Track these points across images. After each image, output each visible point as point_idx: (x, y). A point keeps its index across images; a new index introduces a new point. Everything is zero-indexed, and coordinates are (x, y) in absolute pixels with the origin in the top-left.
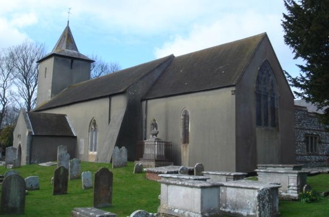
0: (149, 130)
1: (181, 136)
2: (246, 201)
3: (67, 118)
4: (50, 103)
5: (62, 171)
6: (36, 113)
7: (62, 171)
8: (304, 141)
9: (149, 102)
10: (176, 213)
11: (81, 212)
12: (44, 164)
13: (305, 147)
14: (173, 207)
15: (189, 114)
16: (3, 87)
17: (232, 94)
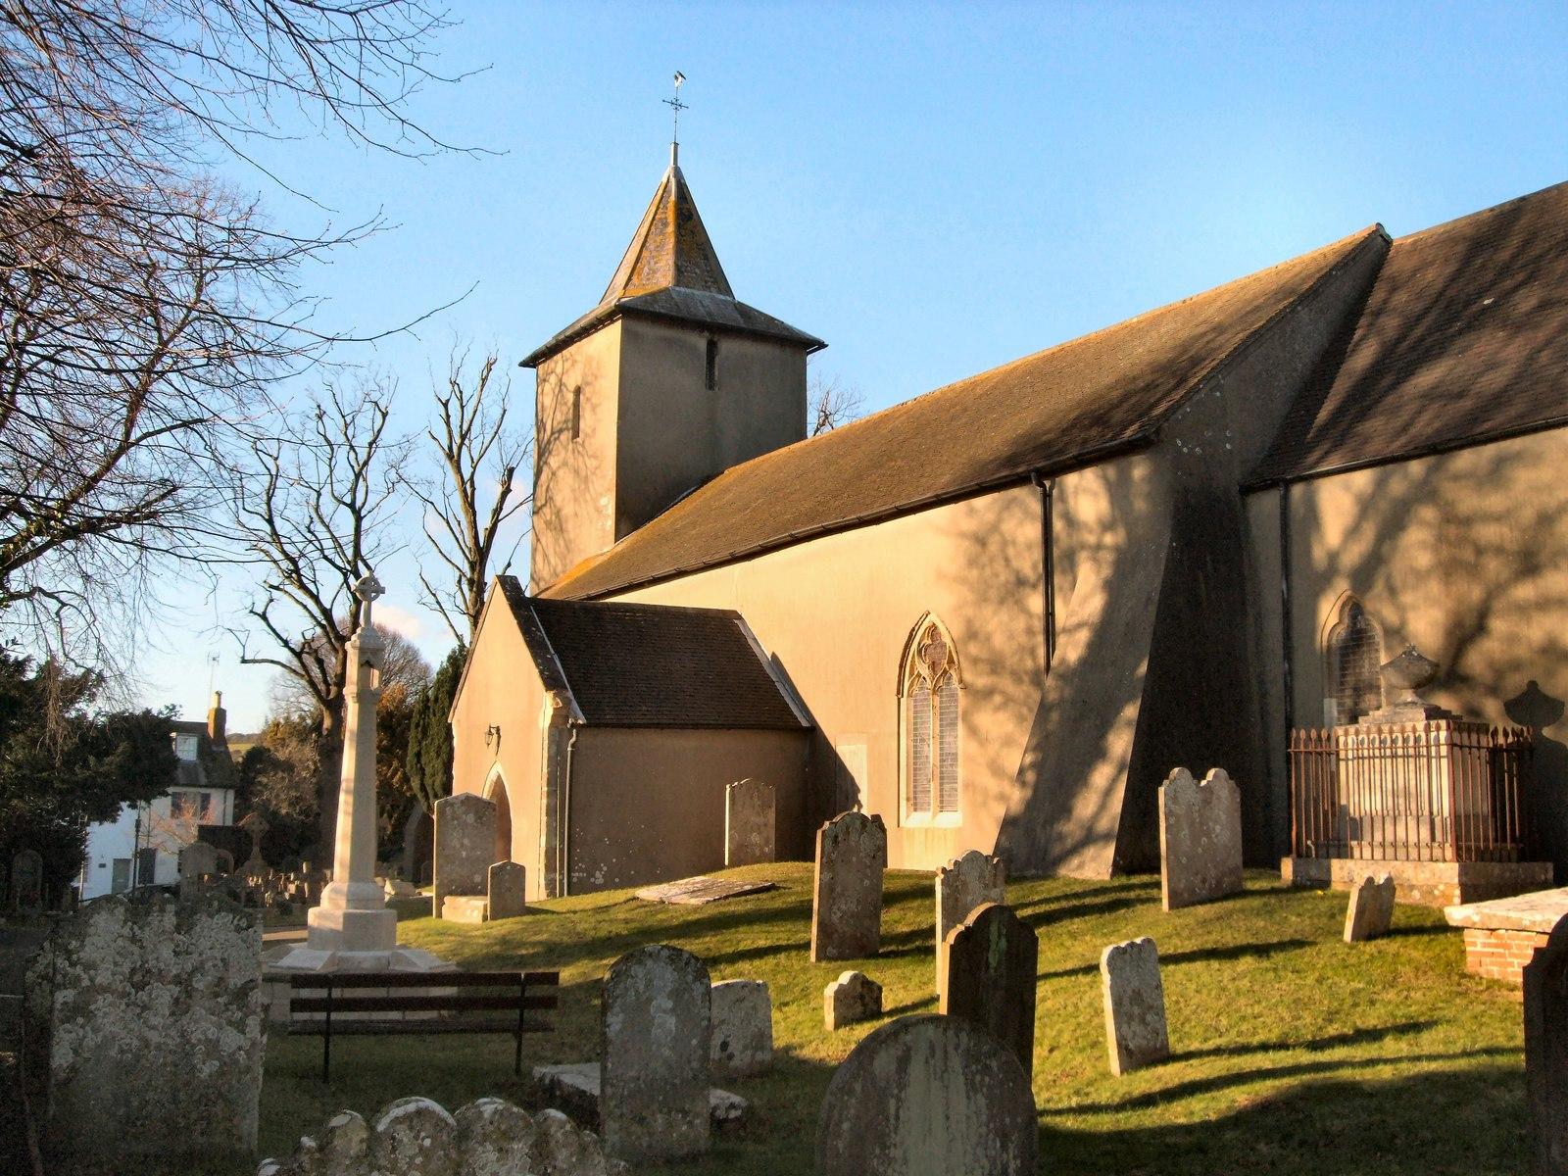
16: (352, 506)
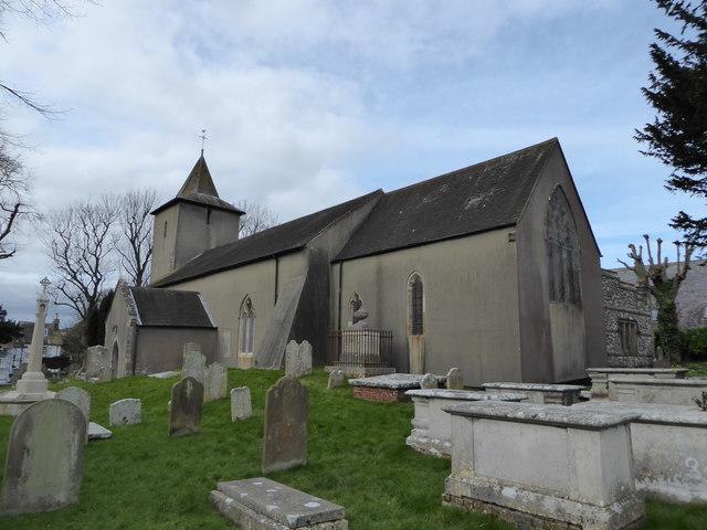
0: (347, 312)
1: (409, 322)
2: (683, 459)
5: (189, 388)
7: (189, 388)
8: (618, 331)
9: (345, 264)
10: (508, 499)
11: (238, 499)
12: (159, 375)
15: (423, 281)
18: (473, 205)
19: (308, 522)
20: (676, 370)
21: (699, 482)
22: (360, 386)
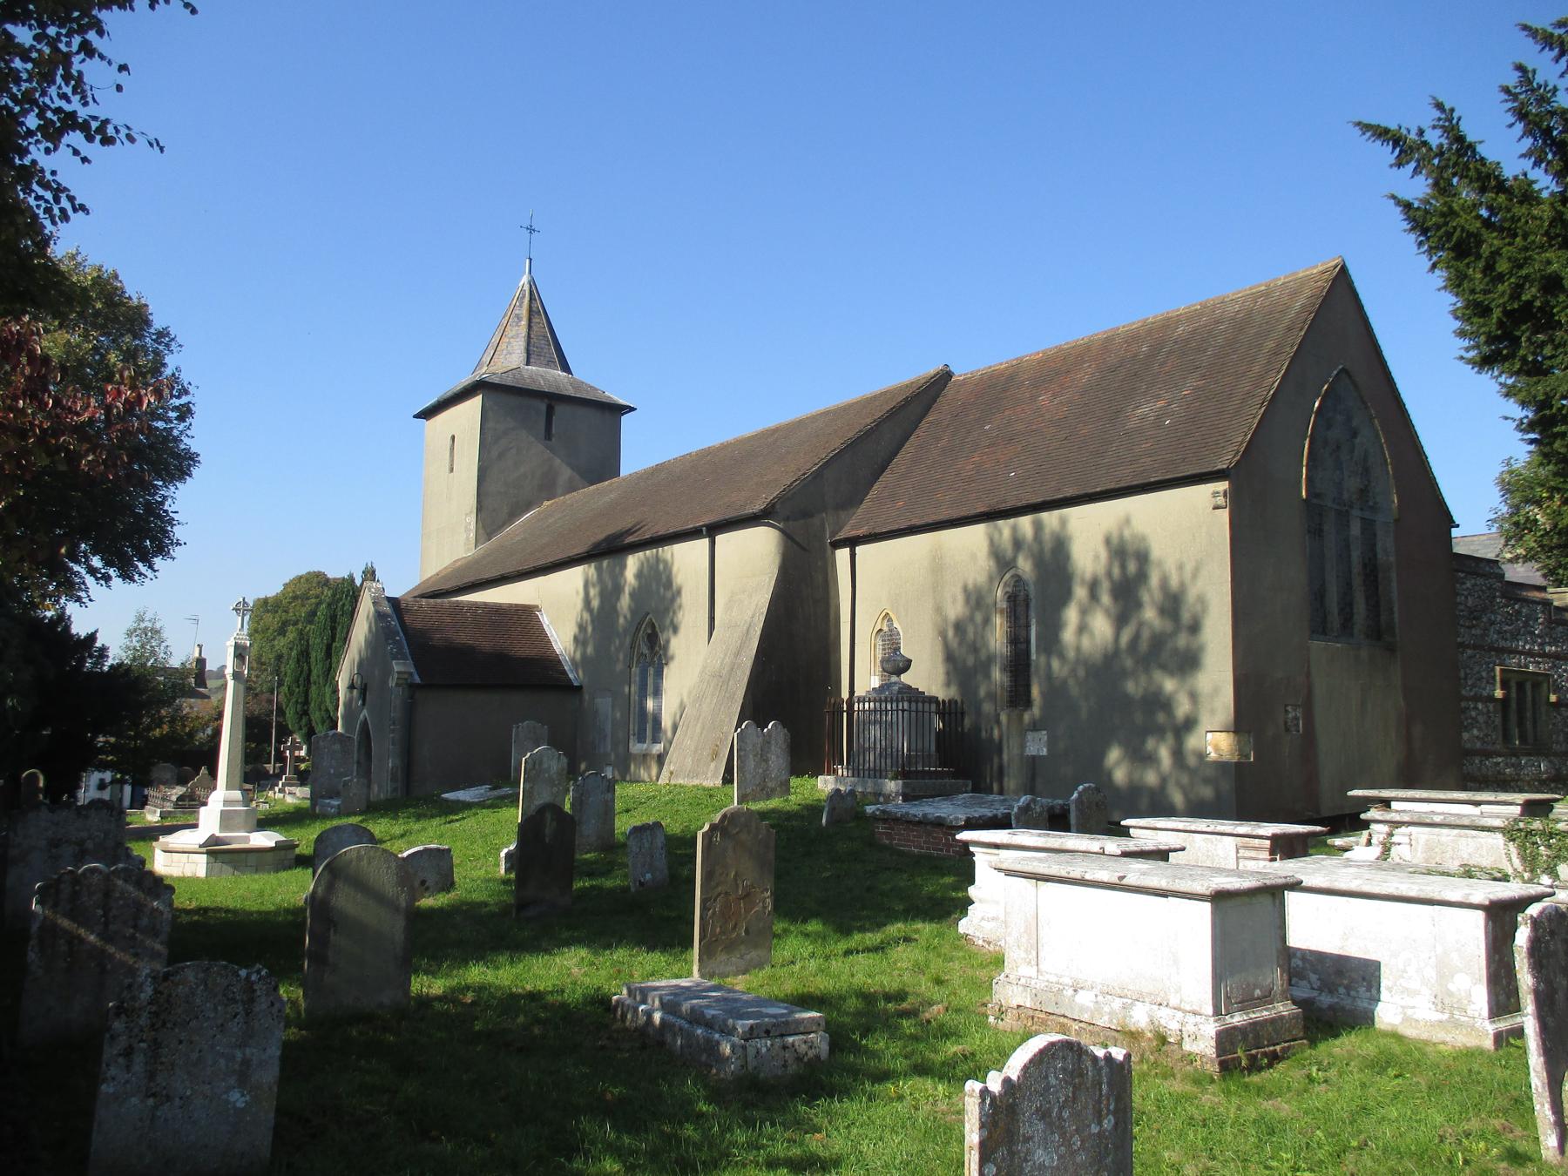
3: (545, 619)
4: (470, 565)
6: (424, 601)
9: (720, 539)
10: (1082, 1009)
13: (1498, 721)
14: (1067, 981)
17: (1216, 508)
18: (1143, 418)
19: (767, 1032)
20: (1270, 829)
21: (1417, 993)
22: (889, 819)
